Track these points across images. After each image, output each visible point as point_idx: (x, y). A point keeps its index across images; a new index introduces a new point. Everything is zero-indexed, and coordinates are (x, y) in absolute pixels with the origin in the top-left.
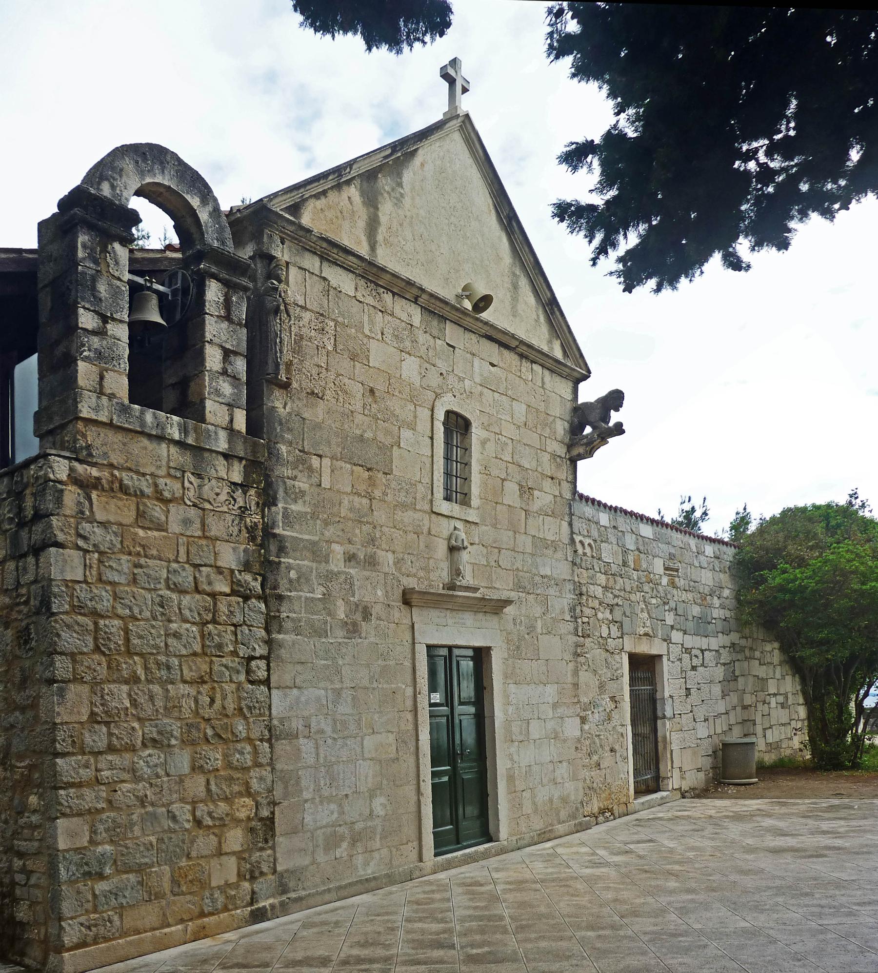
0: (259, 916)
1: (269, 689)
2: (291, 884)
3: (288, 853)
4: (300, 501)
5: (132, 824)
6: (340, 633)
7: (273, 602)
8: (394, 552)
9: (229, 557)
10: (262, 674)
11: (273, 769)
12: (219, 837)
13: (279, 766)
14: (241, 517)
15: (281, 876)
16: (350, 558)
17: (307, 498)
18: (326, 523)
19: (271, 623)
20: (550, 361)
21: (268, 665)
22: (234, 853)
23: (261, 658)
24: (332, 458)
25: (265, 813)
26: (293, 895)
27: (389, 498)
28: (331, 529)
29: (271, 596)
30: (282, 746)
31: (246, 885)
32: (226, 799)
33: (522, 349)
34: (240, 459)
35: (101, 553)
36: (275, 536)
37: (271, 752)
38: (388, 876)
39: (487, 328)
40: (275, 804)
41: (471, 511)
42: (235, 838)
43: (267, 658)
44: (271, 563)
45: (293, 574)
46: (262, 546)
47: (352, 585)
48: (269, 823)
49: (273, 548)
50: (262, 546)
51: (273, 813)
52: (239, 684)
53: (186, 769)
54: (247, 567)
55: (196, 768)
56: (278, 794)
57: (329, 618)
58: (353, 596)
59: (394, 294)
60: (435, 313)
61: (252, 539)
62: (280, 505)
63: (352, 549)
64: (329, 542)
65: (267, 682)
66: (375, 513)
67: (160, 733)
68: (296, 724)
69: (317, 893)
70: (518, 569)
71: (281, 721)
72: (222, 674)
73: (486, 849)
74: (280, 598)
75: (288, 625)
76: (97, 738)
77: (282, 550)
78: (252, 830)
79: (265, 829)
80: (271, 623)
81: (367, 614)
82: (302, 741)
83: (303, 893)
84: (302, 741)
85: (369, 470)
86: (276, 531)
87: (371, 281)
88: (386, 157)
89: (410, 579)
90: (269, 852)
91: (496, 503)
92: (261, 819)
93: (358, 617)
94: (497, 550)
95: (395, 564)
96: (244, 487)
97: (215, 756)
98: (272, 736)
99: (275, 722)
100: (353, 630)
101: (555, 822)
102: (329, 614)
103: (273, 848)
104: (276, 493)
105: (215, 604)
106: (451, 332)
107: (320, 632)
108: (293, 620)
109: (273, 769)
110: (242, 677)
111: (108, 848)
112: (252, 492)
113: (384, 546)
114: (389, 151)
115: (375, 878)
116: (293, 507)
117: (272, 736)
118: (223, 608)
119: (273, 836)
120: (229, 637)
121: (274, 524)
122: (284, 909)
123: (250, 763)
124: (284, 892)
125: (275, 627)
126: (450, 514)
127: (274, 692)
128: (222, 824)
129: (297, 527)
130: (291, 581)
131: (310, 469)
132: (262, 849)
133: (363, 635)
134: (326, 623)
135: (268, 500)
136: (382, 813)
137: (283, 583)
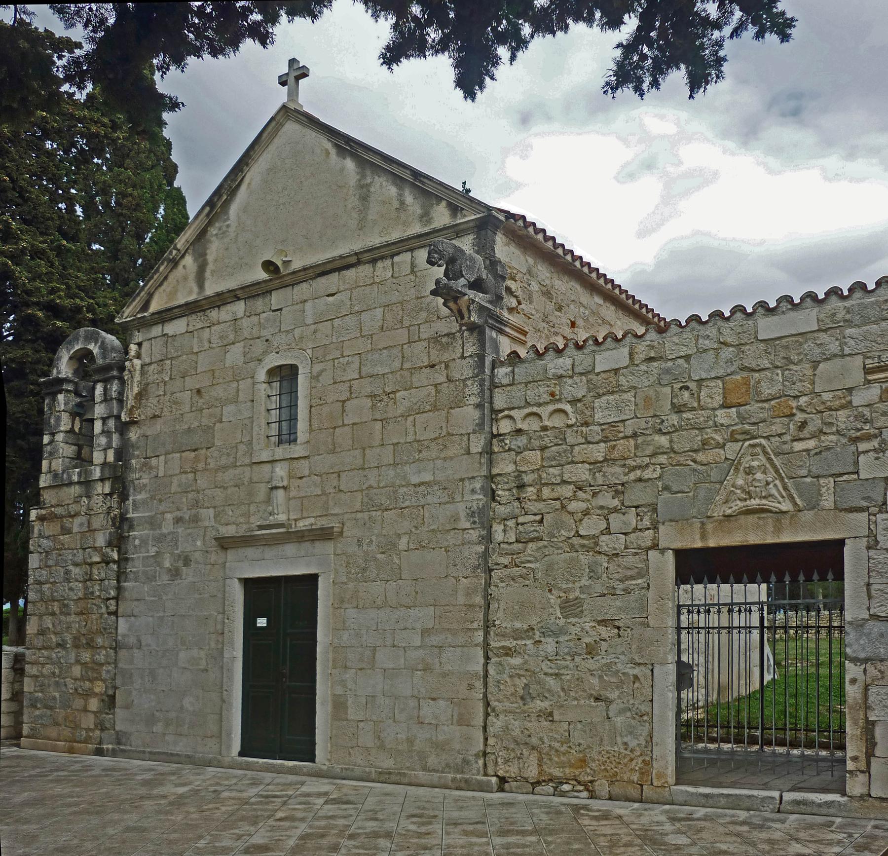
0: (99, 752)
1: (117, 617)
2: (124, 740)
3: (121, 719)
4: (143, 492)
5: (49, 686)
6: (166, 577)
7: (123, 564)
8: (214, 507)
9: (101, 540)
10: (113, 608)
11: (116, 667)
12: (86, 701)
13: (120, 665)
14: (108, 513)
15: (117, 733)
16: (178, 521)
17: (148, 488)
18: (160, 501)
19: (121, 576)
20: (413, 241)
21: (117, 603)
22: (93, 712)
23: (113, 598)
24: (165, 454)
25: (110, 692)
26: (122, 747)
27: (212, 465)
28: (164, 504)
29: (123, 560)
30: (123, 653)
31: (98, 732)
32: (89, 680)
33: (366, 257)
34: (109, 478)
35: (47, 552)
36: (127, 518)
37: (116, 656)
38: (187, 756)
39: (311, 271)
40: (116, 688)
41: (298, 448)
42: (94, 704)
43: (116, 598)
44: (124, 537)
45: (137, 542)
46: (119, 528)
47: (177, 541)
48: (113, 698)
49: (126, 528)
50: (119, 528)
51: (115, 693)
52: (102, 614)
53: (72, 661)
54: (110, 544)
55: (78, 662)
56: (118, 682)
57: (158, 568)
58: (177, 549)
59: (219, 307)
60: (259, 295)
61: (114, 525)
62: (131, 499)
63: (179, 514)
64: (163, 513)
65: (115, 613)
66: (199, 482)
67: (63, 640)
68: (132, 640)
69: (136, 751)
70: (370, 486)
71: (124, 636)
72: (91, 608)
73: (295, 766)
74: (127, 559)
75: (131, 576)
76: (38, 642)
77: (131, 527)
78: (103, 701)
79: (110, 702)
80: (121, 576)
81: (187, 561)
82: (135, 650)
83: (129, 748)
84: (135, 650)
85: (194, 451)
86: (128, 516)
87: (199, 312)
88: (208, 215)
89: (229, 527)
90: (111, 716)
91: (335, 428)
92: (108, 696)
93: (180, 564)
94: (335, 475)
95: (215, 517)
96: (111, 494)
97: (86, 656)
98: (116, 647)
99: (120, 638)
100: (175, 573)
101: (417, 767)
102: (158, 566)
103: (113, 714)
104: (129, 491)
105: (91, 570)
106: (276, 299)
107: (151, 578)
108: (134, 573)
109: (116, 667)
110: (104, 610)
111: (40, 694)
112: (115, 496)
113: (206, 505)
114: (208, 209)
115: (178, 755)
116: (139, 497)
117: (116, 647)
118: (95, 571)
119: (114, 707)
120: (97, 587)
121: (127, 512)
122: (114, 753)
123: (103, 661)
124: (119, 743)
125: (123, 578)
126: (271, 459)
127: (120, 619)
128: (88, 694)
129: (141, 509)
130: (135, 547)
131: (151, 468)
132: (107, 714)
133: (184, 577)
134: (155, 572)
135: (124, 497)
136: (191, 709)
137: (131, 548)
